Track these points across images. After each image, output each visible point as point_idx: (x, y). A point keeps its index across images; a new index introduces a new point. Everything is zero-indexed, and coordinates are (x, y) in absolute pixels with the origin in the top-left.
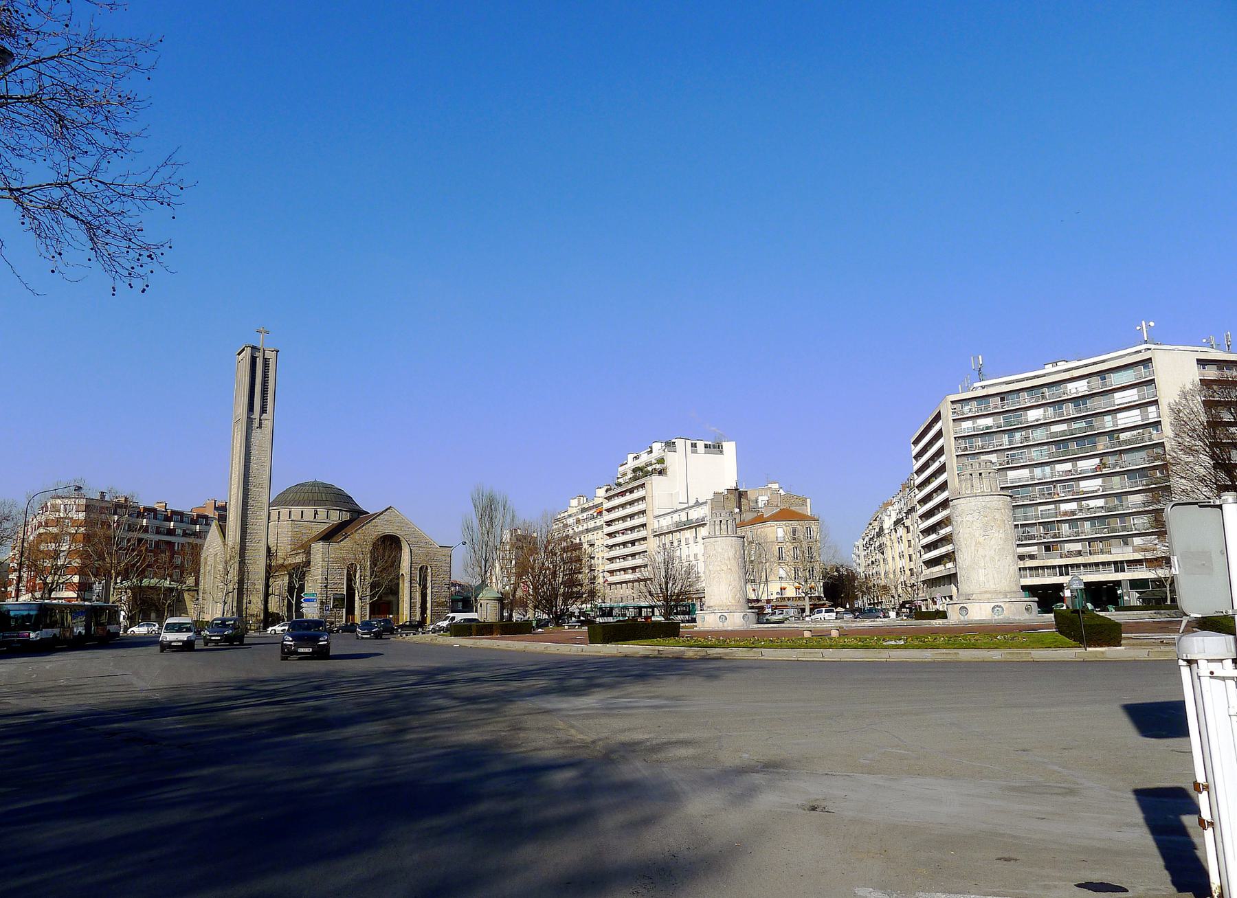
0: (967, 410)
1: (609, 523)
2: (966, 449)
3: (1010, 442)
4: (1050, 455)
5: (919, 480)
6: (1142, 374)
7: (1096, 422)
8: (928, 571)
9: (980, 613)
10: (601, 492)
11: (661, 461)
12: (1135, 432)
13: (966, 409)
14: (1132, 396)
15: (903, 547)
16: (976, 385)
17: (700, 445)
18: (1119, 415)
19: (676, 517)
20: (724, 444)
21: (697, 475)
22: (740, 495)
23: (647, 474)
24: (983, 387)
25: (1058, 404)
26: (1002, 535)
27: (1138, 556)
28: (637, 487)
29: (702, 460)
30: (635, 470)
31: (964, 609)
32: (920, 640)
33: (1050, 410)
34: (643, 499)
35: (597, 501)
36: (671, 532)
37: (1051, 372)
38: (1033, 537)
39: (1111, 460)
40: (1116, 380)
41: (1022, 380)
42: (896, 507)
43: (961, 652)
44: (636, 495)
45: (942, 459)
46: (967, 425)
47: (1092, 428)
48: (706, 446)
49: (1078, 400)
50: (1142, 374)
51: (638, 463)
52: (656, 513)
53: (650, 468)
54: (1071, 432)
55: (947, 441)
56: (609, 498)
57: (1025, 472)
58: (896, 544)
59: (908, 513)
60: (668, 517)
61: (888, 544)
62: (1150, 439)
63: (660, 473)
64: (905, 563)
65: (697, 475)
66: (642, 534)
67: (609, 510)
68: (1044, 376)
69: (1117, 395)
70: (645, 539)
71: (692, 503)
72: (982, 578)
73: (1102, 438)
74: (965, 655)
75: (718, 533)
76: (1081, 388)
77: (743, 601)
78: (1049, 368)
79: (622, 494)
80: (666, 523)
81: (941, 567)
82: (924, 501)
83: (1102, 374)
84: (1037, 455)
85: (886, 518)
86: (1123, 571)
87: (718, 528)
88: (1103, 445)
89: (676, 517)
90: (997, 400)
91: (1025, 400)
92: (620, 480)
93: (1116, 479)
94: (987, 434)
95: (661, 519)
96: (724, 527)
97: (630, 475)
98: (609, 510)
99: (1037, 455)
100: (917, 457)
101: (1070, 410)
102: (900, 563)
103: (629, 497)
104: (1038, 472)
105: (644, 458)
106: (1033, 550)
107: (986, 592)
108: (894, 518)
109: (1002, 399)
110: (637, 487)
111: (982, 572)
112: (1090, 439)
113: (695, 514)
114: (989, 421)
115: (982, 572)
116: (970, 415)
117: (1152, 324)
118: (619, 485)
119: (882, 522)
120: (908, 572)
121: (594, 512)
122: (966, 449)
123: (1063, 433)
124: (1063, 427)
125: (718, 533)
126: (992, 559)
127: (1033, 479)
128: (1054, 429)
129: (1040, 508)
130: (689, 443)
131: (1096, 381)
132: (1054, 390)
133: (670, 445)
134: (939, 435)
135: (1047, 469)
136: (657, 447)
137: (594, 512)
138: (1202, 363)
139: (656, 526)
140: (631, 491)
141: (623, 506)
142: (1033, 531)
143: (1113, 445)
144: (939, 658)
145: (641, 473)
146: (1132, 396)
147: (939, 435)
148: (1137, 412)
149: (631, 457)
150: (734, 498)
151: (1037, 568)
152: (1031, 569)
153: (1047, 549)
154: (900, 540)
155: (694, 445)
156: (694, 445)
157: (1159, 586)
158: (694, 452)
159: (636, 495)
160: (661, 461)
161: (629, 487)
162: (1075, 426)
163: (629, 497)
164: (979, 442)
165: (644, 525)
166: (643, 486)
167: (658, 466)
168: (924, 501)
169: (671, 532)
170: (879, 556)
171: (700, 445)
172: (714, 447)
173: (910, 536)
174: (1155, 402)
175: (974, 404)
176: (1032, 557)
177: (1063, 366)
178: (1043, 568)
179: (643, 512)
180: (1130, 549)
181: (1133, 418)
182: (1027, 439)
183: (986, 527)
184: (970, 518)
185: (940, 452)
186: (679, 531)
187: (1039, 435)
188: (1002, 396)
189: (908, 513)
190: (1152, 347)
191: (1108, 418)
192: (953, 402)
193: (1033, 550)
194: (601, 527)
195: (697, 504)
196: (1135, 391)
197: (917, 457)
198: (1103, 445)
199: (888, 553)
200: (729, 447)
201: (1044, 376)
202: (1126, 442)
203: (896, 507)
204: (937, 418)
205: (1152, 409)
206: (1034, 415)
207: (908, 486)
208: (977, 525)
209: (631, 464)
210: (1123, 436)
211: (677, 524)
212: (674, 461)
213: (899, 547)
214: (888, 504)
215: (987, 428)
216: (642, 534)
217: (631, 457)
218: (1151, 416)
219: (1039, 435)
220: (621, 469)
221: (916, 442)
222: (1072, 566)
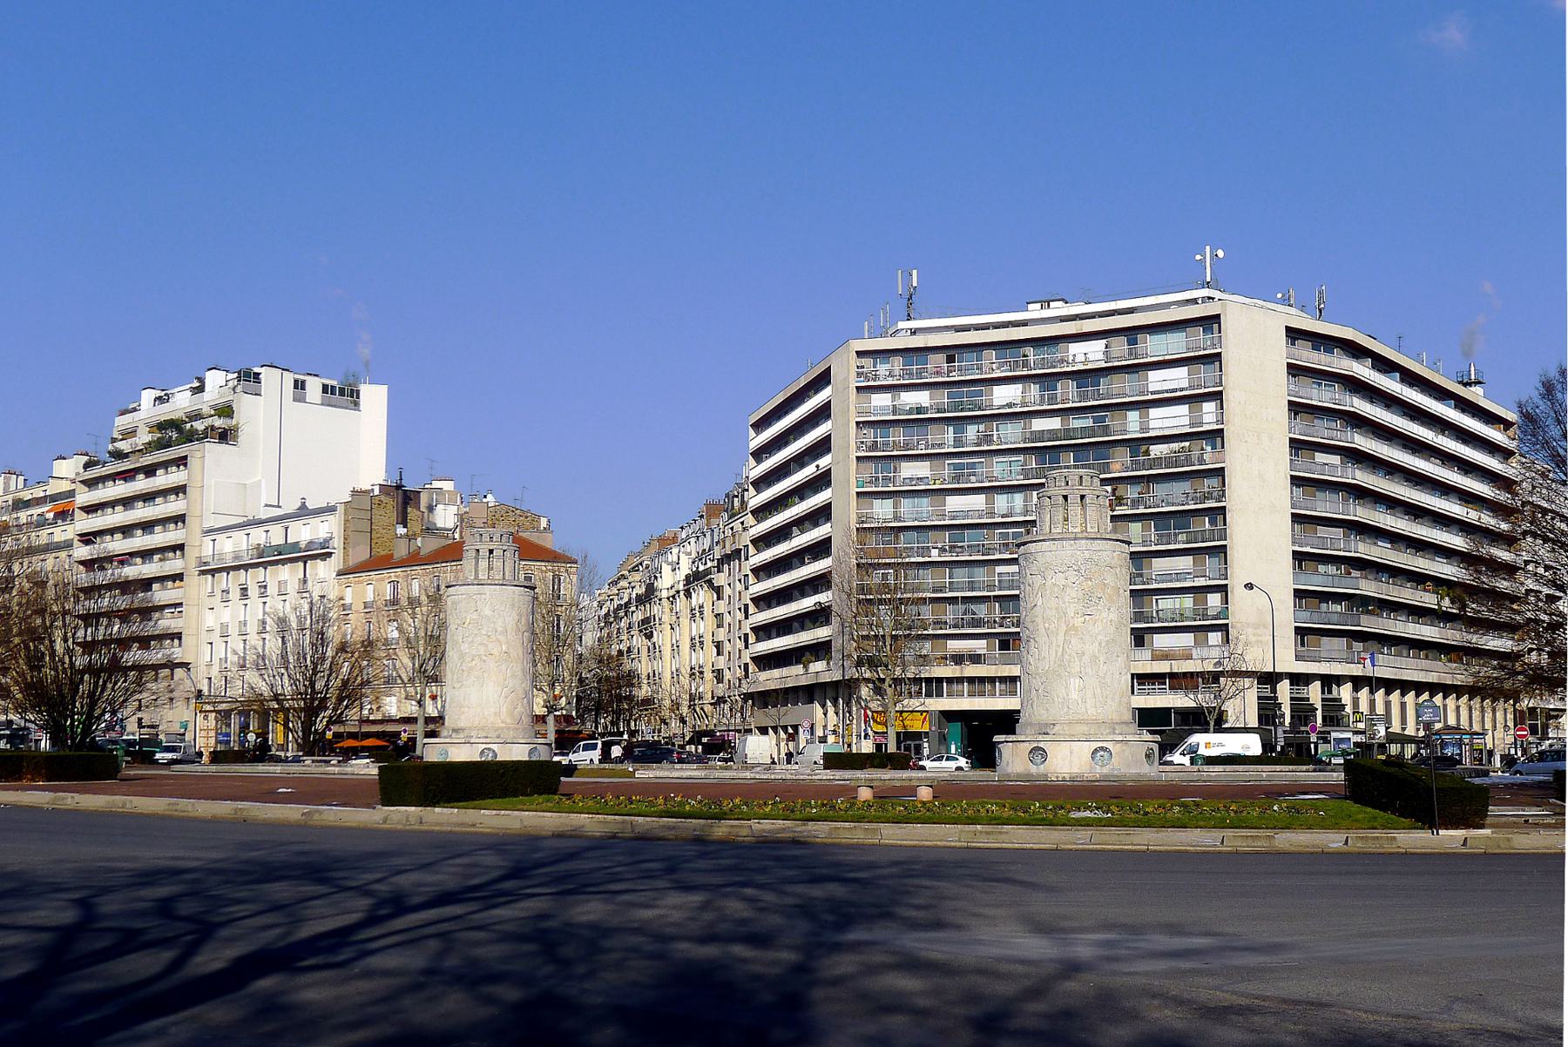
0: (884, 371)
1: (87, 538)
2: (874, 447)
3: (958, 442)
4: (1026, 473)
5: (756, 499)
6: (1198, 342)
7: (1112, 420)
8: (764, 675)
9: (1068, 761)
10: (68, 469)
11: (226, 411)
12: (1175, 446)
13: (883, 369)
14: (1177, 379)
15: (705, 627)
16: (902, 325)
17: (314, 386)
18: (1154, 412)
19: (258, 536)
20: (365, 390)
21: (306, 451)
22: (403, 498)
23: (191, 436)
24: (914, 332)
25: (1047, 380)
26: (1113, 616)
27: (1162, 667)
28: (165, 465)
29: (316, 418)
30: (162, 426)
31: (1038, 753)
32: (393, 789)
33: (1034, 389)
34: (180, 490)
35: (54, 488)
36: (246, 567)
37: (1040, 318)
38: (977, 623)
39: (1131, 492)
40: (1156, 347)
41: (979, 327)
42: (692, 547)
43: (573, 816)
44: (162, 480)
45: (824, 462)
46: (882, 400)
47: (1106, 430)
48: (325, 388)
49: (1086, 377)
50: (1198, 342)
51: (166, 412)
52: (207, 525)
53: (199, 426)
54: (1068, 433)
55: (842, 430)
56: (91, 484)
57: (979, 501)
58: (685, 621)
59: (727, 559)
60: (239, 535)
61: (665, 618)
62: (1202, 461)
63: (225, 436)
64: (707, 657)
65: (306, 451)
66: (173, 565)
67: (90, 509)
68: (1024, 323)
69: (1154, 375)
70: (178, 577)
71: (290, 506)
72: (1074, 695)
73: (1120, 449)
74: (1288, 840)
75: (483, 576)
76: (1090, 354)
77: (526, 720)
78: (1035, 311)
79: (127, 476)
80: (232, 546)
81: (798, 669)
82: (763, 541)
83: (1131, 333)
84: (1002, 470)
85: (666, 569)
86: (982, 694)
87: (483, 564)
88: (1120, 465)
89: (258, 536)
90: (941, 358)
91: (991, 365)
92: (124, 446)
93: (1136, 527)
94: (917, 422)
95: (220, 537)
96: (497, 564)
97: (144, 437)
98: (90, 509)
99: (1002, 470)
100: (760, 454)
101: (1068, 393)
102: (687, 658)
103: (141, 484)
104: (1001, 501)
105: (182, 402)
106: (979, 646)
107: (1079, 722)
108: (685, 569)
109: (950, 359)
110: (165, 465)
111: (1075, 683)
112: (1102, 450)
113: (303, 532)
114: (922, 398)
115: (1075, 683)
116: (890, 382)
117: (1221, 253)
118: (119, 455)
119: (655, 574)
120: (708, 675)
121: (47, 511)
122: (874, 447)
123: (1053, 434)
124: (1054, 423)
125: (483, 576)
126: (1094, 659)
127: (992, 514)
128: (1039, 424)
129: (999, 569)
130: (289, 378)
131: (1120, 345)
132: (1046, 354)
133: (249, 378)
134: (823, 412)
135: (1018, 498)
136: (214, 379)
137: (47, 511)
138: (1294, 334)
139: (207, 550)
140: (150, 471)
141: (127, 502)
142: (981, 611)
143: (1137, 465)
144: (1244, 846)
145: (174, 433)
146: (1177, 379)
147: (823, 412)
148: (1183, 409)
149: (148, 396)
150: (391, 504)
151: (982, 680)
152: (971, 680)
153: (1005, 645)
154: (696, 614)
155: (299, 385)
156: (299, 385)
157: (1332, 718)
158: (299, 399)
159: (162, 480)
160: (226, 411)
161: (147, 460)
162: (1077, 423)
163: (141, 484)
164: (898, 435)
165: (180, 547)
166: (182, 461)
167: (219, 422)
168: (763, 541)
169: (246, 567)
170: (638, 641)
171: (314, 386)
172: (342, 393)
173: (722, 607)
174: (1217, 396)
175: (897, 363)
176: (976, 659)
177: (1058, 309)
178: (992, 680)
179: (179, 519)
180: (1147, 654)
181: (1172, 419)
182: (988, 439)
183: (1088, 598)
184: (1060, 579)
185: (823, 446)
186: (265, 565)
187: (1010, 435)
188: (952, 353)
189: (727, 559)
190: (1216, 294)
191: (1133, 416)
192: (860, 354)
193: (979, 646)
194: (68, 545)
195: (303, 512)
196: (1182, 372)
197: (760, 454)
198: (1120, 465)
199: (663, 638)
200: (374, 396)
201: (1024, 323)
202: (1157, 462)
203: (692, 547)
204: (823, 379)
205: (1209, 407)
206: (1004, 395)
207: (729, 507)
208: (1072, 593)
209: (148, 408)
210: (1157, 450)
211: (261, 551)
212: (253, 413)
213: (687, 630)
214: (666, 543)
215: (919, 410)
216: (173, 565)
217: (148, 396)
218: (1206, 419)
219: (1010, 435)
220: (122, 422)
221: (760, 425)
222: (950, 680)
